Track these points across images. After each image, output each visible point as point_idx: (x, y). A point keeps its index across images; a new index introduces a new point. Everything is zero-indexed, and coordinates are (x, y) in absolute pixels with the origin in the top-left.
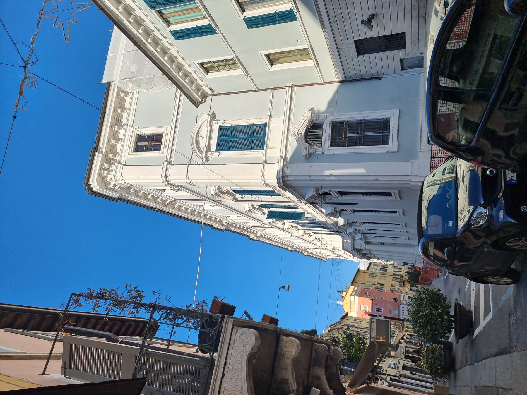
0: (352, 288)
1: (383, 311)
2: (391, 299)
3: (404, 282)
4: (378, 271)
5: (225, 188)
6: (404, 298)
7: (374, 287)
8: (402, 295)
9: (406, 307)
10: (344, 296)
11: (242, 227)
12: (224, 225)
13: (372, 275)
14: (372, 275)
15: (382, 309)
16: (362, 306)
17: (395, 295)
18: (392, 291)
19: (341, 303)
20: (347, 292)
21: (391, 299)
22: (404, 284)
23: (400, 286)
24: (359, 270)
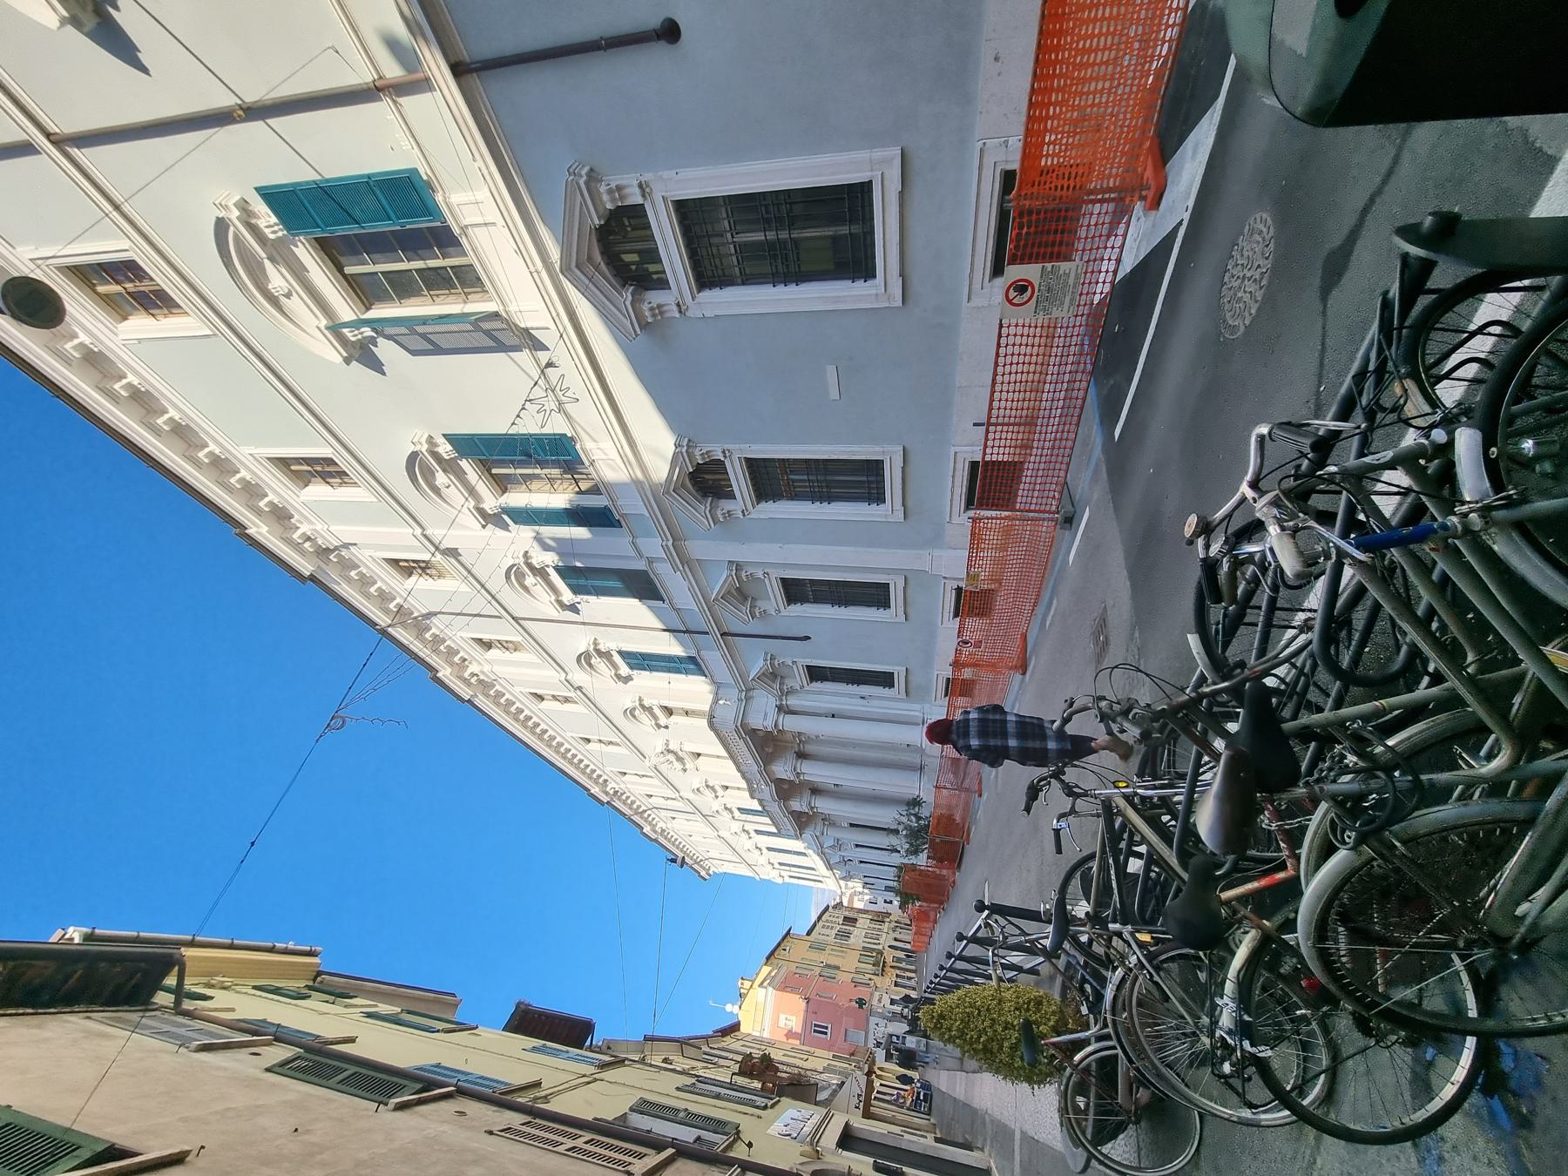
0: (766, 970)
1: (829, 1031)
2: (851, 1000)
3: (884, 966)
4: (831, 939)
5: (650, 701)
6: (880, 1001)
7: (818, 970)
8: (877, 995)
9: (882, 1022)
10: (746, 991)
11: (635, 806)
12: (607, 793)
13: (818, 947)
14: (818, 947)
15: (827, 1028)
16: (782, 1017)
17: (862, 992)
18: (856, 984)
19: (735, 1009)
20: (753, 981)
21: (851, 1000)
22: (883, 970)
23: (874, 974)
24: (788, 933)
